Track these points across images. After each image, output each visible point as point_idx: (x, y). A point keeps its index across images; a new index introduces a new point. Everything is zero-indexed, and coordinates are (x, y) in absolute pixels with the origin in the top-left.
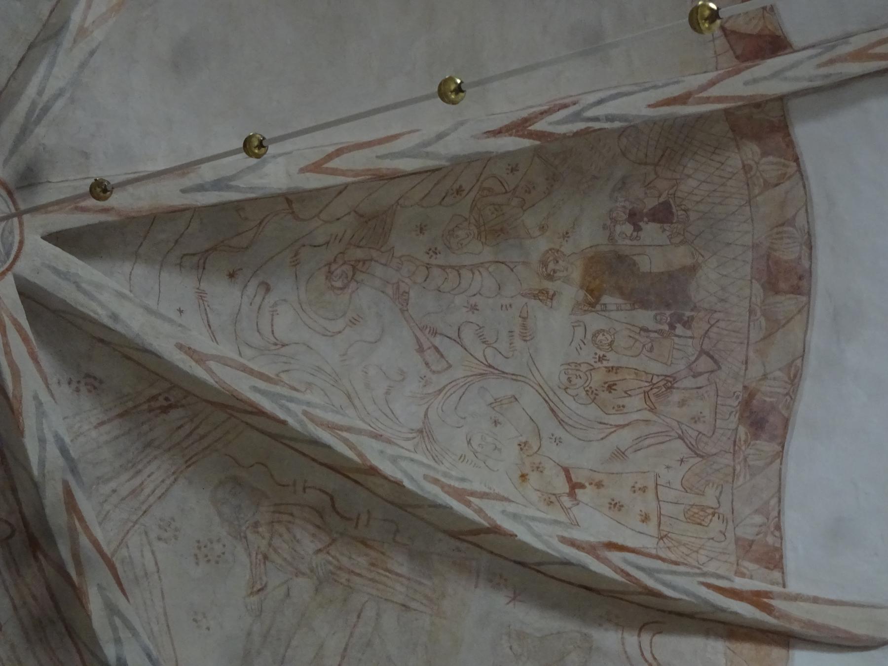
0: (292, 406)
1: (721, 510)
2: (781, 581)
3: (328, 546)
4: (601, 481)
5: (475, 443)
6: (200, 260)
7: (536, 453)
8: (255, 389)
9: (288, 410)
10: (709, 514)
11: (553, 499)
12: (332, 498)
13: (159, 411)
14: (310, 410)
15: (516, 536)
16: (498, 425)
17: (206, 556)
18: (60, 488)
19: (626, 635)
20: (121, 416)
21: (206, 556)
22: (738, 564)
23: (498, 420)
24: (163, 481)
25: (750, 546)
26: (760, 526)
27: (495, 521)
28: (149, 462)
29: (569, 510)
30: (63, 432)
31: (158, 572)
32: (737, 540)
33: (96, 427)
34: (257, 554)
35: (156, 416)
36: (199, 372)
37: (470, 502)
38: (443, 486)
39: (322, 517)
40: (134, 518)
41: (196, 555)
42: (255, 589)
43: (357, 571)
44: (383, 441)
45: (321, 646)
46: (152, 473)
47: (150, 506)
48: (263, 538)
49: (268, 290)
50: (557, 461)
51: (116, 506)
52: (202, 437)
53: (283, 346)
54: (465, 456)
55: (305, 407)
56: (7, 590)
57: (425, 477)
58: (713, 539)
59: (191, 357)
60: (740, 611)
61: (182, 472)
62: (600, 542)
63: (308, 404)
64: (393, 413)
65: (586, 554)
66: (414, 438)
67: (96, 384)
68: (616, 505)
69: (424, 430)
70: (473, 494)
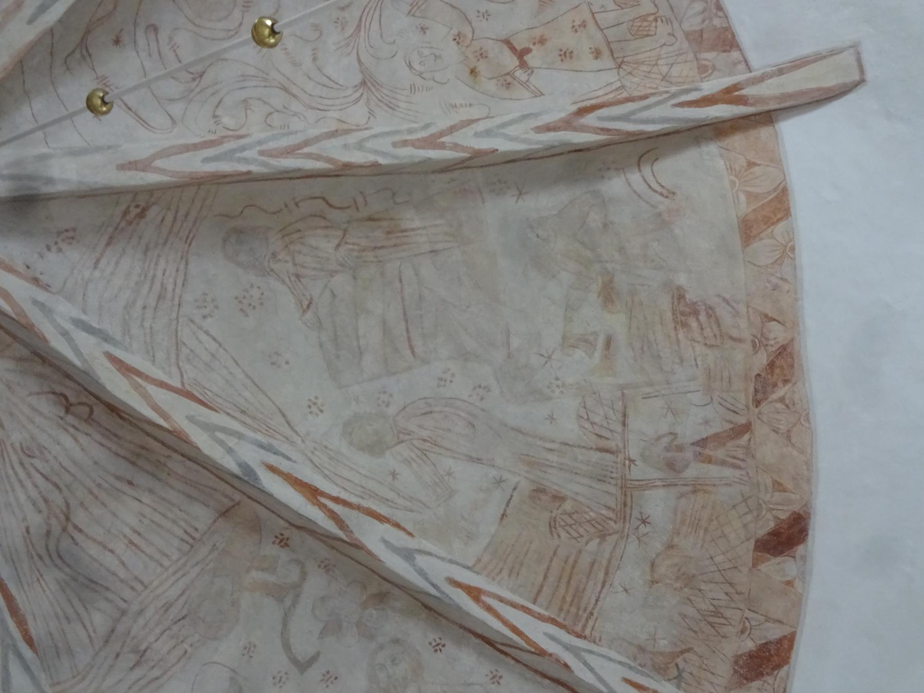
0: (247, 154)
1: (661, 13)
2: (741, 59)
3: (343, 238)
4: (542, 36)
5: (416, 66)
6: (81, 51)
7: (472, 39)
8: (206, 160)
9: (246, 160)
10: (652, 22)
11: (509, 79)
12: (323, 199)
14: (264, 147)
15: (497, 150)
16: (427, 32)
17: (250, 305)
19: (629, 176)
20: (108, 244)
21: (250, 305)
22: (697, 59)
23: (424, 25)
24: (177, 270)
25: (701, 36)
26: (703, 12)
27: (473, 148)
28: (156, 264)
29: (528, 83)
30: (76, 313)
31: (220, 345)
32: (687, 35)
33: (95, 267)
34: (289, 278)
35: (138, 224)
36: (152, 178)
37: (443, 143)
38: (414, 144)
39: (324, 218)
40: (174, 315)
41: (241, 310)
42: (305, 307)
43: (379, 245)
44: (341, 135)
45: (384, 322)
47: (180, 297)
48: (287, 262)
49: (155, 29)
50: (494, 37)
52: (187, 215)
53: (201, 76)
54: (414, 84)
55: (258, 148)
57: (395, 145)
58: (664, 44)
59: (136, 169)
60: (718, 114)
61: (187, 252)
62: (570, 115)
63: (260, 143)
64: (331, 80)
65: (563, 132)
66: (362, 94)
67: (71, 234)
68: (566, 55)
69: (366, 80)
70: (442, 134)
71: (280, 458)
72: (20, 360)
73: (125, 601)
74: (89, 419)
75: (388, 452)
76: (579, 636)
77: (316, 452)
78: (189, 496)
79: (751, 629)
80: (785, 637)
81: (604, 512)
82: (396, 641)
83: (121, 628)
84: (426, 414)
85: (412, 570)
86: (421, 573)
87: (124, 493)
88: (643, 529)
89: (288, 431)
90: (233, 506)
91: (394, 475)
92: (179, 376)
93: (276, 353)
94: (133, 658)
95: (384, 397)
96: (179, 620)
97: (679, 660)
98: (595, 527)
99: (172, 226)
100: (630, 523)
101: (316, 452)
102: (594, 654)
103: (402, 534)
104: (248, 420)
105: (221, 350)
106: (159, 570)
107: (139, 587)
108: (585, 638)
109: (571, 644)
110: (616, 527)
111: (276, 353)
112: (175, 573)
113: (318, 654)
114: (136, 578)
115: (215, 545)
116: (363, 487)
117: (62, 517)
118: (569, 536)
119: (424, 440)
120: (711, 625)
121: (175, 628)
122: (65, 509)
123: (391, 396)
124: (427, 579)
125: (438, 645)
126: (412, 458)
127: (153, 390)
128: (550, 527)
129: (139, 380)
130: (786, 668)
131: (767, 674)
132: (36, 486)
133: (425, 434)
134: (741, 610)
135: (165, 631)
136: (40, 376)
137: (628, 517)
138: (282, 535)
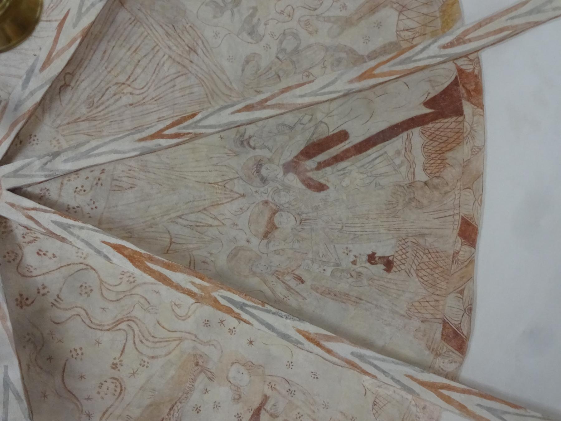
72: (44, 112)
73: (164, 55)
74: (72, 74)
83: (178, 59)
94: (192, 53)
96: (175, 29)
106: (149, 37)
107: (157, 48)
112: (151, 30)
114: (153, 49)
117: (123, 86)
121: (178, 31)
129: (54, 54)
135: (179, 36)
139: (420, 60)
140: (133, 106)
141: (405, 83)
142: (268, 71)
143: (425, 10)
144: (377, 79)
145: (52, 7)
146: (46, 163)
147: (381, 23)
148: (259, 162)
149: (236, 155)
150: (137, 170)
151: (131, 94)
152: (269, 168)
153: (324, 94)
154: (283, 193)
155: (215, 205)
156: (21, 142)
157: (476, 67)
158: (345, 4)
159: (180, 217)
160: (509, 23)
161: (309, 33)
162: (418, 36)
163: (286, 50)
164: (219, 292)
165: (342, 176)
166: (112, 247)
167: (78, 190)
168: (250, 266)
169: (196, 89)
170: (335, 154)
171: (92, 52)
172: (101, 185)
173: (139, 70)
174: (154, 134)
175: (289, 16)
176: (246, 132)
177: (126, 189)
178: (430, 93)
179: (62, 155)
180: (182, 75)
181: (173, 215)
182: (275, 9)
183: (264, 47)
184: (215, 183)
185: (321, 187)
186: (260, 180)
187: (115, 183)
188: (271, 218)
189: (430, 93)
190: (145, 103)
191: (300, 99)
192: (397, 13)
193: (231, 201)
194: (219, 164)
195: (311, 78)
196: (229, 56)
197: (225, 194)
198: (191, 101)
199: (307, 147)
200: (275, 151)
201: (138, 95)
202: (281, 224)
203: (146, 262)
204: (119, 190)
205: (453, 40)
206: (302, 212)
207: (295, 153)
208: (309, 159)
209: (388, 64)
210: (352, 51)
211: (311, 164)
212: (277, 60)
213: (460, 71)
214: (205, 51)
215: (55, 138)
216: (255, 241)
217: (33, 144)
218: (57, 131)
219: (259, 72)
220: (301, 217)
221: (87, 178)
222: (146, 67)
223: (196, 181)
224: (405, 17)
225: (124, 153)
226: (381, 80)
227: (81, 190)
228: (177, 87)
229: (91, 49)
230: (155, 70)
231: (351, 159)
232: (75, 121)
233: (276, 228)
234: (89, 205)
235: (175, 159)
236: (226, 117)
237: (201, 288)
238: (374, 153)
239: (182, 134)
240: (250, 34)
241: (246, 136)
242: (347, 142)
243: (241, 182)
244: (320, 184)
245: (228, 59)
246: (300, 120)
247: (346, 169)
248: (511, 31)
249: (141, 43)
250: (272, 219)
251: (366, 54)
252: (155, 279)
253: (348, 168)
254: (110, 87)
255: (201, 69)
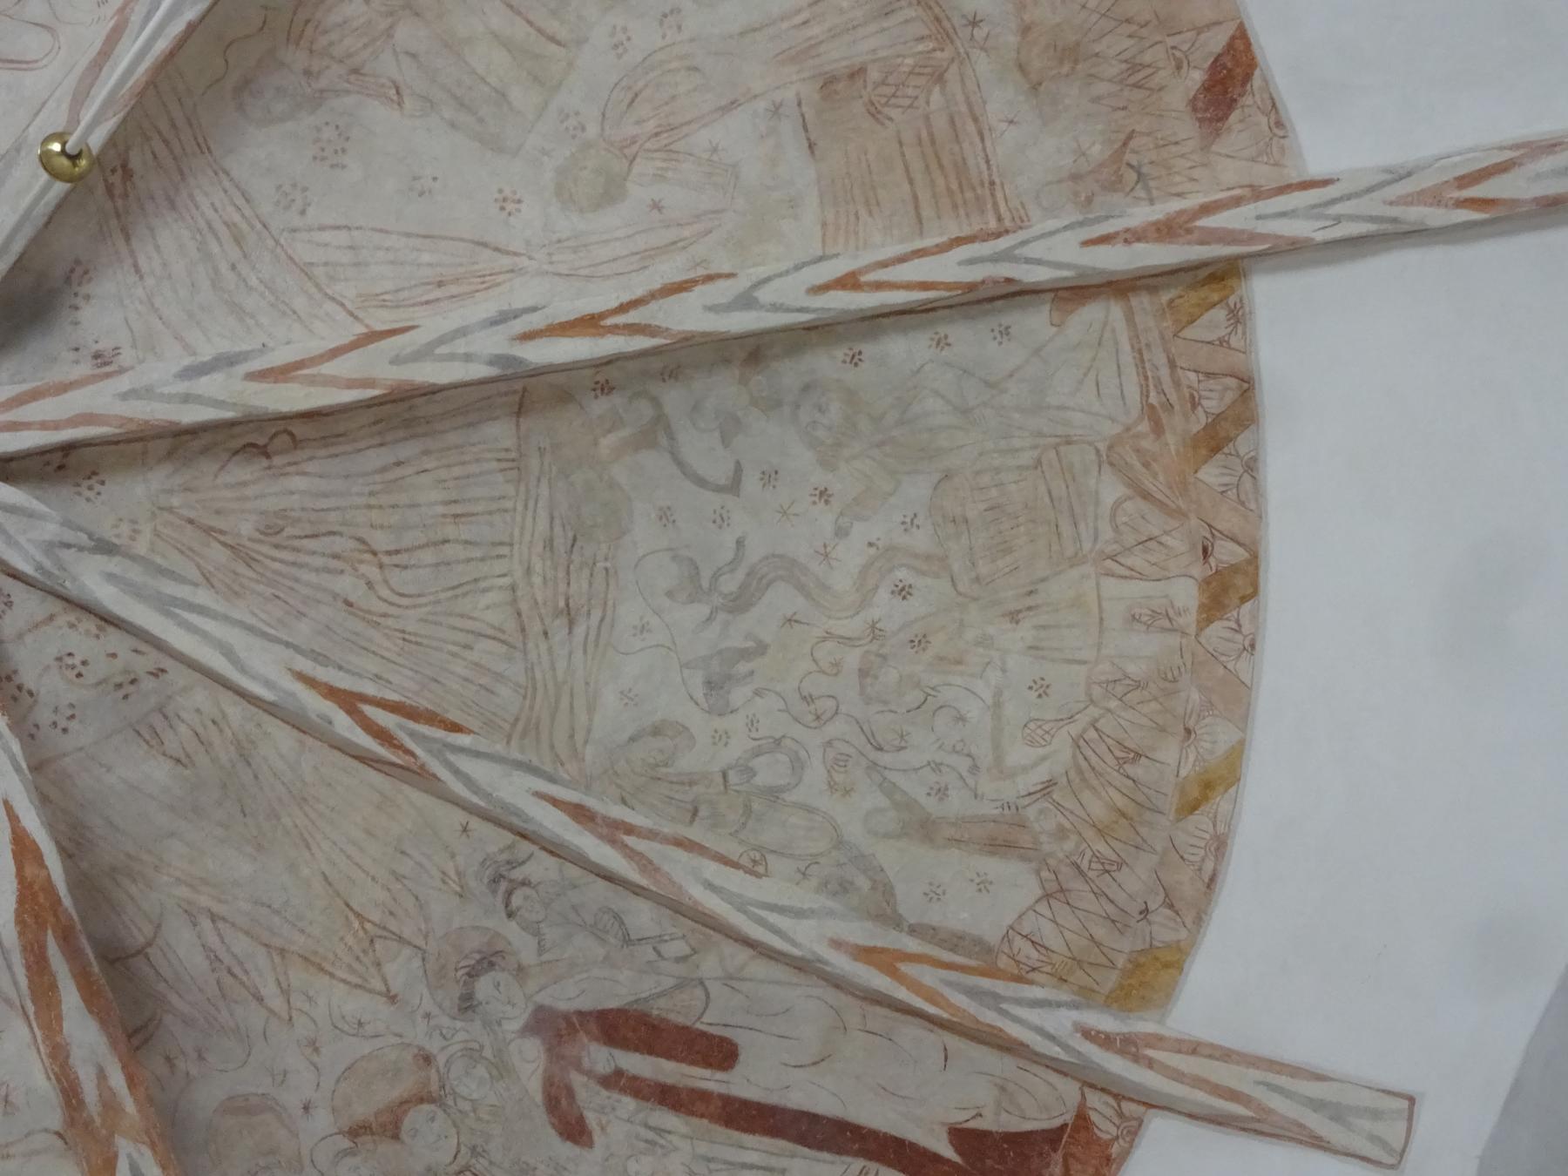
13: (128, 183)
17: (336, 152)
18: (254, 386)
20: (128, 238)
24: (226, 191)
31: (349, 228)
33: (141, 278)
40: (270, 243)
41: (332, 166)
42: (395, 98)
45: (495, 36)
46: (213, 204)
47: (257, 217)
51: (254, 268)
56: (360, 450)
71: (526, 318)
72: (170, 455)
73: (504, 575)
74: (296, 443)
75: (629, 184)
76: (998, 235)
77: (555, 258)
78: (470, 425)
79: (1186, 57)
80: (1233, 38)
81: (921, 47)
82: (807, 388)
83: (524, 606)
84: (633, 101)
85: (763, 314)
86: (776, 308)
87: (403, 478)
88: (979, 33)
89: (506, 261)
90: (523, 396)
91: (656, 206)
92: (339, 308)
93: (415, 179)
94: (561, 622)
95: (572, 122)
96: (573, 546)
97: (1129, 157)
98: (923, 74)
99: (171, 152)
100: (959, 37)
101: (555, 258)
102: (1031, 242)
103: (721, 284)
104: (454, 289)
105: (355, 233)
107: (505, 550)
108: (1007, 232)
109: (997, 251)
110: (946, 54)
111: (415, 179)
112: (526, 507)
113: (738, 463)
114: (494, 544)
115: (540, 448)
116: (637, 253)
117: (368, 556)
118: (900, 109)
119: (657, 134)
120: (1137, 86)
121: (576, 557)
122: (362, 547)
123: (577, 114)
124: (789, 310)
125: (853, 357)
126: (662, 169)
127: (329, 369)
128: (873, 115)
130: (1257, 73)
131: (1241, 95)
132: (314, 553)
133: (650, 126)
134: (1161, 42)
135: (569, 567)
136: (205, 451)
137: (951, 31)
138: (597, 383)
139: (1016, 1020)
140: (350, 609)
141: (945, 1049)
142: (683, 783)
143: (1100, 932)
144: (896, 984)
145: (384, 300)
146: (68, 546)
147: (991, 883)
148: (492, 955)
149: (461, 896)
150: (230, 734)
151: (370, 584)
152: (501, 988)
153: (761, 922)
154: (481, 1071)
155: (311, 962)
156: (61, 467)
157: (1123, 1139)
158: (947, 789)
159: (214, 918)
160: (1259, 1093)
161: (829, 783)
162: (1047, 973)
163: (755, 775)
164: (139, 1151)
165: (642, 1145)
166: (14, 831)
167: (70, 661)
168: (257, 1165)
169: (505, 691)
170: (670, 1081)
171: (377, 440)
172: (126, 697)
173: (428, 556)
174: (339, 690)
175: (818, 718)
176: (528, 863)
177: (164, 754)
178: (981, 1115)
179: (117, 559)
180: (503, 642)
181: (204, 901)
182: (801, 682)
183: (716, 731)
184: (358, 915)
185: (575, 1130)
186: (460, 999)
187: (157, 721)
188: (405, 1104)
189: (981, 1115)
190: (379, 624)
191: (702, 888)
192: (1039, 892)
193: (357, 986)
194: (406, 882)
195: (761, 869)
196: (630, 690)
197: (358, 958)
198: (473, 702)
199: (621, 1012)
200: (549, 962)
201: (380, 598)
202: (414, 1136)
203: (50, 932)
204: (148, 743)
205: (1118, 1034)
206: (484, 1151)
207: (586, 1004)
208: (605, 1044)
209: (944, 973)
210: (888, 891)
211: (602, 1058)
212: (720, 780)
213: (1083, 1118)
214: (592, 637)
215: (134, 522)
216: (323, 1121)
217: (79, 494)
218: (154, 514)
219: (664, 770)
220: (474, 1161)
221: (114, 655)
222: (449, 564)
223: (323, 873)
224: (1048, 914)
225: (243, 670)
226: (902, 994)
227: (73, 667)
228: (473, 656)
229: (380, 433)
230: (461, 585)
231: (695, 1121)
232: (209, 531)
233: (396, 1137)
234: (56, 710)
235: (330, 785)
236: (516, 791)
237: (110, 1104)
238: (756, 1150)
239: (395, 742)
240: (710, 684)
241: (517, 874)
242: (719, 1075)
243: (417, 963)
244: (581, 1120)
245: (622, 693)
246: (661, 939)
247: (666, 1135)
248: (1250, 1114)
249: (483, 514)
250: (405, 1107)
251: (912, 921)
252: (29, 988)
253: (670, 1137)
254: (341, 534)
255: (553, 668)
